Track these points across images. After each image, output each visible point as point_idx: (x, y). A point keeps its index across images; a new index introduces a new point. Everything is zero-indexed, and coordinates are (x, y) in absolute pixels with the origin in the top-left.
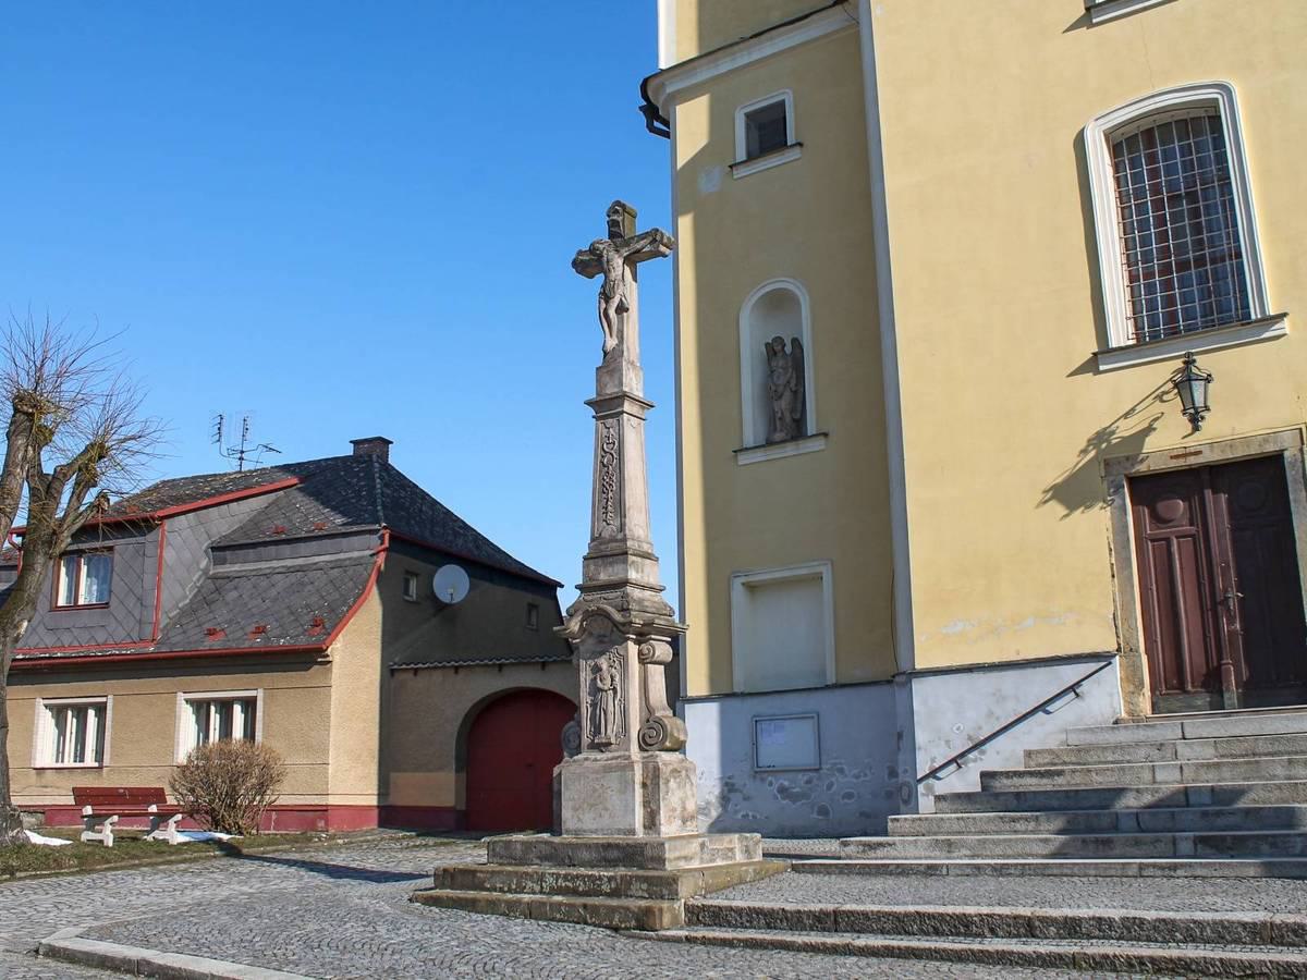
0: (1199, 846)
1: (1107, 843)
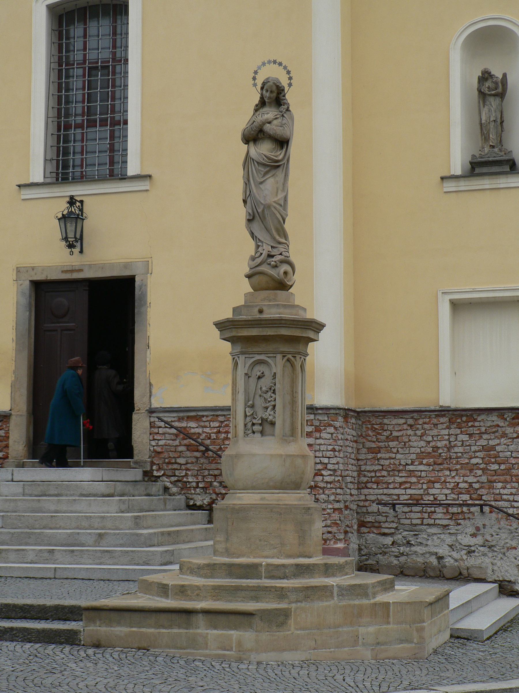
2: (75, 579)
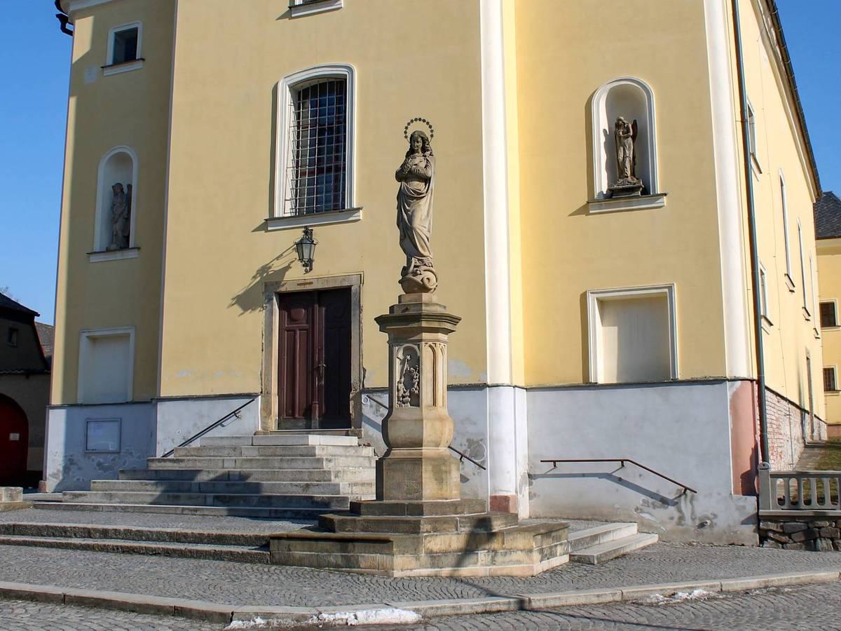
0: (216, 500)
1: (177, 497)
2: (779, 304)
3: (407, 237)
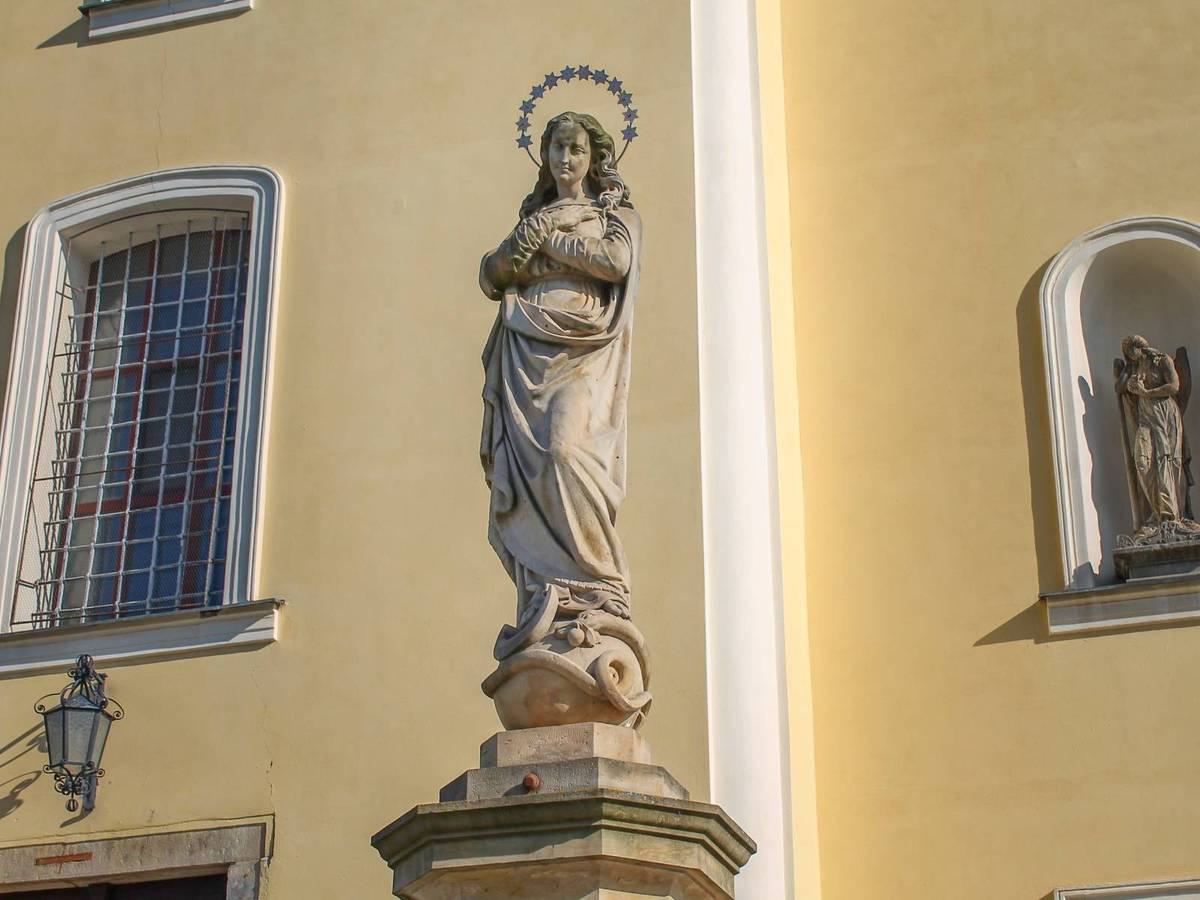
3: (526, 503)
